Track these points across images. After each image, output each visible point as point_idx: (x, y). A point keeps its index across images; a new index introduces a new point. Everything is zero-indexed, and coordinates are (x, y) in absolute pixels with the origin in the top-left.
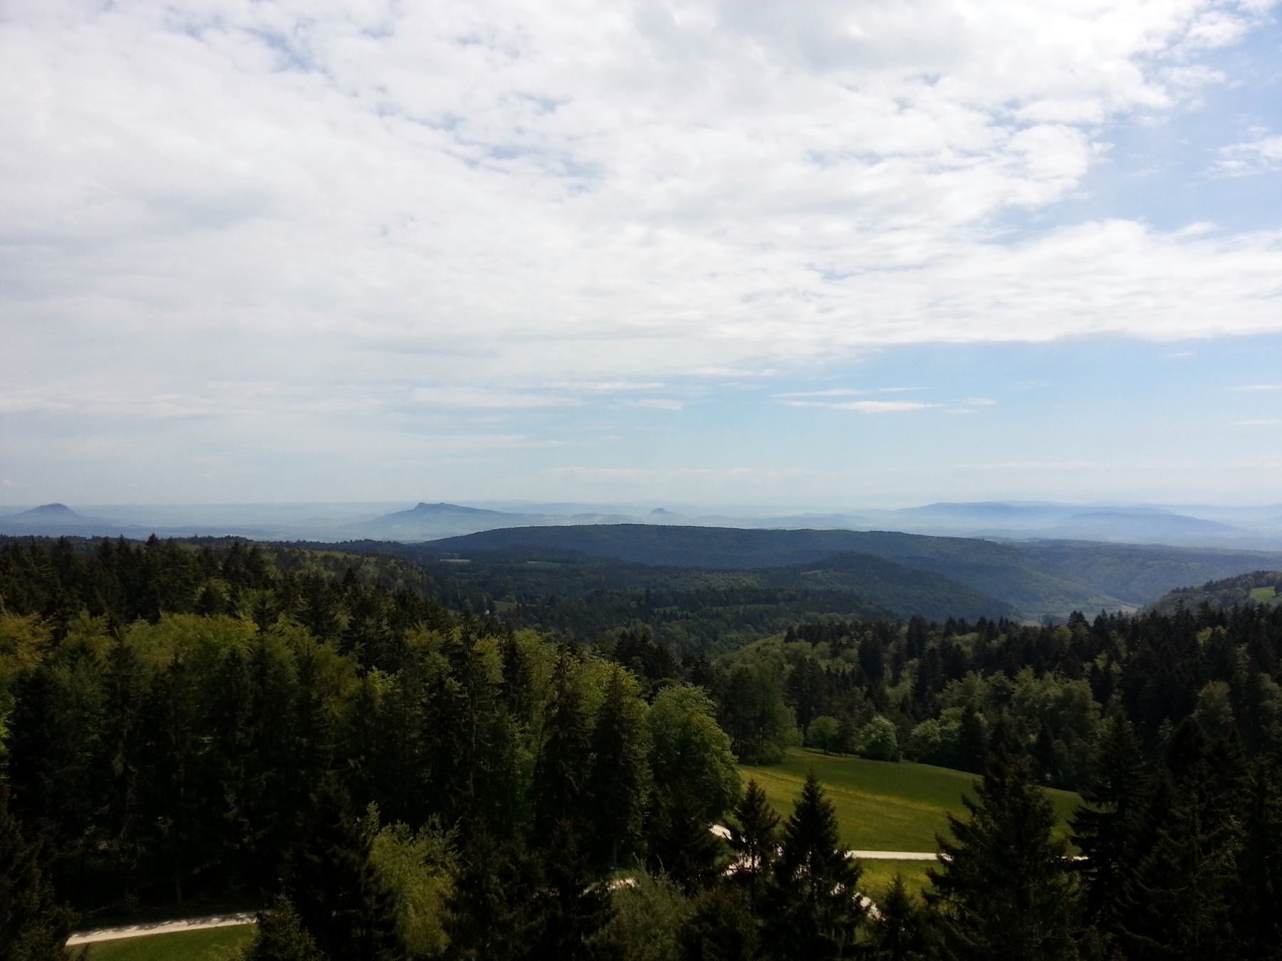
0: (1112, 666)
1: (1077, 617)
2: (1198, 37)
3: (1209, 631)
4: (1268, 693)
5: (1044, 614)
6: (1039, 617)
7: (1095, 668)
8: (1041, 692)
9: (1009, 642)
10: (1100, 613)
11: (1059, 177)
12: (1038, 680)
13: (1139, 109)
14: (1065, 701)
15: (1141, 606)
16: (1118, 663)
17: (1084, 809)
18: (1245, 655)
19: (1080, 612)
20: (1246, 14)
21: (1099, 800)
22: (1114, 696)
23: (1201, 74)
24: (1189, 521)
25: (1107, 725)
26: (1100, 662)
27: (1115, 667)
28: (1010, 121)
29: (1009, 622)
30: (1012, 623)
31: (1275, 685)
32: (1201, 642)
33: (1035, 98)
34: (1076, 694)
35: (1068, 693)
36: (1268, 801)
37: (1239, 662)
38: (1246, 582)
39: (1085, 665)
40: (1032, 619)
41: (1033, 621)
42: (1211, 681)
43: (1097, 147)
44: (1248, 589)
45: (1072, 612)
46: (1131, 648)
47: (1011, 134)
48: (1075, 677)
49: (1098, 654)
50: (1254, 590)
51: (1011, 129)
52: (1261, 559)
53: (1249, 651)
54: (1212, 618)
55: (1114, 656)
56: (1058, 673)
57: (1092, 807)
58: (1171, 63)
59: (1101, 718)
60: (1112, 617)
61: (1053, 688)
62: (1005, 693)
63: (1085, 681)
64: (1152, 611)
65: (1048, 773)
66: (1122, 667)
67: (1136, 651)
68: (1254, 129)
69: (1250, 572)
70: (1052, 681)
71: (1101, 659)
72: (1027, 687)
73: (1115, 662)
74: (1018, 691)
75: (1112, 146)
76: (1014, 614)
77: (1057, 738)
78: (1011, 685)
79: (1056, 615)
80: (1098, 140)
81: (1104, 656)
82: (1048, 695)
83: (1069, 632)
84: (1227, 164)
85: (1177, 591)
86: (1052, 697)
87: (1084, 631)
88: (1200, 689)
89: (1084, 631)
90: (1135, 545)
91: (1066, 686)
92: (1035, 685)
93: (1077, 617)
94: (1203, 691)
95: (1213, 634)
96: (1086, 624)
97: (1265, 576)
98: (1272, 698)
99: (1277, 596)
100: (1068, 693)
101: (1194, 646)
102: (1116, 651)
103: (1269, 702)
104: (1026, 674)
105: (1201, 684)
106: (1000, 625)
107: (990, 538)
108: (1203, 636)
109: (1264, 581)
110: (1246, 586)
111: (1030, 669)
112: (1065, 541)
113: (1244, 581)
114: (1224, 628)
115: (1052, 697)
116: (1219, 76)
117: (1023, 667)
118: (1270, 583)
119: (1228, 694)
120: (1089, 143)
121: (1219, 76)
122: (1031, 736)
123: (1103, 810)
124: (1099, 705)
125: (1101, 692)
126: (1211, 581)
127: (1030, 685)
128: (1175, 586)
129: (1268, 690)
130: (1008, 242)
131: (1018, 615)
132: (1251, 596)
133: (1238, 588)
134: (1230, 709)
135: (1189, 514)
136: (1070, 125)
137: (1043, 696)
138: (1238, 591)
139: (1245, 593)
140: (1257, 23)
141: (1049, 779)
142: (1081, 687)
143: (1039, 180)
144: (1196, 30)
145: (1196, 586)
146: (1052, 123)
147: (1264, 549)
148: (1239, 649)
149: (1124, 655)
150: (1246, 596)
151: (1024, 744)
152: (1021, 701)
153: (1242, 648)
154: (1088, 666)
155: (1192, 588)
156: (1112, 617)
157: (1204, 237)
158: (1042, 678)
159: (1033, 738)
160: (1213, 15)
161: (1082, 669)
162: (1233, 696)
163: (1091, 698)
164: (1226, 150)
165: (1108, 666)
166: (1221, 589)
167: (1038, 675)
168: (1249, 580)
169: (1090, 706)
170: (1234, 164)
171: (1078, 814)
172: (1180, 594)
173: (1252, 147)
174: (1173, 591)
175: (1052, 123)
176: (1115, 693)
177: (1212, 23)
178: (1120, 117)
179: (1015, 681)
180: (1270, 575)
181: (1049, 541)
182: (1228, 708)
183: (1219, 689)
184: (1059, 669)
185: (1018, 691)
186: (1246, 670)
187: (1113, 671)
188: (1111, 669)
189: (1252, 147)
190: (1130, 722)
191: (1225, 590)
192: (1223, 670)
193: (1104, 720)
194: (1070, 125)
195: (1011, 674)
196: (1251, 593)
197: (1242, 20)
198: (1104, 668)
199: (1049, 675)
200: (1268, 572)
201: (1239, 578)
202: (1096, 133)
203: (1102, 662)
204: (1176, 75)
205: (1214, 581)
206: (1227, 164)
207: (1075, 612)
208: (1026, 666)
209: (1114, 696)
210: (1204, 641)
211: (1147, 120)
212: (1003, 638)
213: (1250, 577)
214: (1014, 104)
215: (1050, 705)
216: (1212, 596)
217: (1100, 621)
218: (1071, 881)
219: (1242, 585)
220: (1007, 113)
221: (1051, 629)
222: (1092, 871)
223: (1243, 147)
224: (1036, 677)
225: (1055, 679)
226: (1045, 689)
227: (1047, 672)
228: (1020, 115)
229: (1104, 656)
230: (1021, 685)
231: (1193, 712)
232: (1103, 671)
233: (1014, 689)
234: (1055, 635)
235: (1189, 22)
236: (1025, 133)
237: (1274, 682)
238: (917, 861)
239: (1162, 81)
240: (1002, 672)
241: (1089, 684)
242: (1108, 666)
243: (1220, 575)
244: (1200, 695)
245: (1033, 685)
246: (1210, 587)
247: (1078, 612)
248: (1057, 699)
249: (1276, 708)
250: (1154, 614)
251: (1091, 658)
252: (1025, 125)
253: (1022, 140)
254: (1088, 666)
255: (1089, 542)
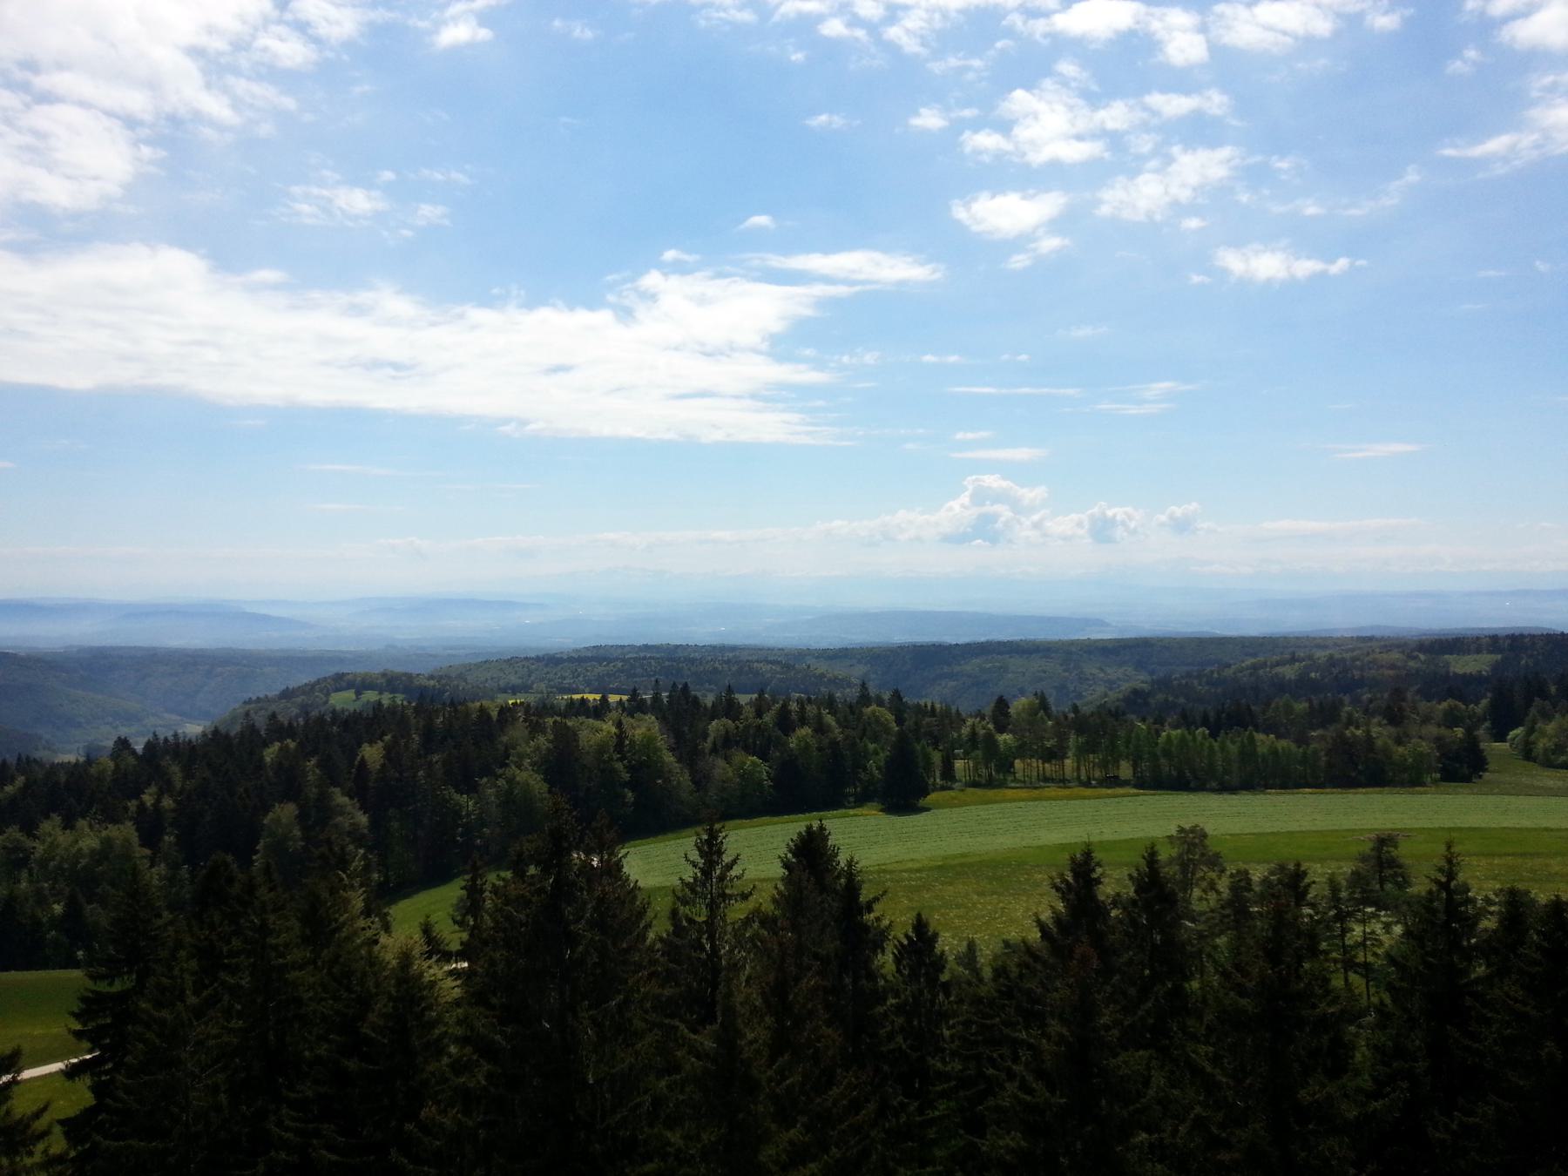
0: (163, 800)
1: (123, 744)
2: (265, 50)
3: (277, 745)
4: (339, 809)
5: (86, 744)
6: (78, 748)
7: (142, 806)
8: (71, 846)
9: (27, 786)
10: (150, 736)
11: (96, 178)
12: (68, 831)
13: (198, 117)
14: (104, 853)
15: (208, 723)
16: (171, 796)
17: (92, 992)
18: (316, 769)
19: (126, 738)
20: (318, 41)
21: (110, 978)
22: (166, 838)
23: (264, 92)
24: (507, 605)
25: (157, 874)
26: (148, 799)
27: (167, 803)
28: (25, 87)
29: (32, 759)
30: (35, 760)
31: (346, 799)
32: (268, 759)
33: (61, 66)
34: (118, 842)
35: (107, 843)
36: (272, 941)
37: (309, 778)
38: (325, 686)
39: (129, 804)
40: (70, 752)
41: (70, 755)
42: (277, 805)
43: (146, 151)
44: (328, 695)
45: (115, 739)
46: (188, 774)
47: (27, 106)
48: (116, 821)
49: (147, 788)
50: (333, 694)
51: (28, 99)
52: (338, 658)
53: (318, 765)
54: (279, 730)
55: (166, 788)
56: (94, 819)
57: (103, 987)
58: (236, 71)
59: (152, 866)
60: (166, 740)
61: (88, 839)
62: (21, 855)
63: (129, 824)
64: (213, 729)
65: (79, 950)
66: (175, 801)
67: (193, 779)
68: (326, 173)
69: (330, 674)
70: (87, 830)
71: (150, 795)
72: (52, 843)
73: (166, 796)
74: (40, 848)
75: (164, 154)
76: (44, 749)
77: (89, 903)
78: (29, 843)
79: (101, 744)
80: (148, 142)
81: (153, 789)
82: (81, 849)
83: (111, 765)
84: (298, 206)
85: (250, 701)
86: (86, 850)
87: (131, 760)
88: (265, 815)
89: (131, 760)
90: (201, 650)
91: (104, 833)
92: (64, 838)
93: (123, 744)
94: (269, 817)
95: (281, 749)
96: (134, 752)
97: (345, 678)
98: (342, 814)
99: (358, 699)
100: (107, 843)
101: (260, 765)
102: (169, 782)
103: (340, 818)
104: (50, 827)
105: (267, 809)
106: (18, 764)
107: (9, 648)
108: (270, 754)
109: (344, 684)
110: (325, 691)
111: (57, 818)
112: (112, 648)
113: (323, 685)
114: (294, 741)
115: (86, 850)
116: (289, 103)
117: (47, 817)
118: (350, 686)
119: (297, 817)
120: (136, 143)
121: (289, 103)
122: (56, 906)
123: (117, 987)
124: (147, 852)
125: (150, 830)
126: (287, 688)
127: (55, 839)
128: (246, 696)
129: (338, 805)
130: (25, 250)
131: (49, 749)
132: (330, 702)
133: (317, 694)
134: (299, 833)
135: (263, 611)
136: (109, 114)
137: (74, 850)
138: (317, 697)
139: (324, 699)
140: (329, 54)
141: (82, 957)
142: (125, 832)
143: (69, 177)
144: (264, 41)
145: (271, 694)
146: (84, 104)
147: (344, 648)
148: (308, 764)
149: (178, 785)
150: (326, 702)
151: (45, 920)
152: (43, 863)
153: (312, 762)
154: (132, 805)
155: (266, 696)
156: (166, 740)
157: (275, 287)
158: (72, 828)
159: (58, 908)
160: (281, 30)
161: (126, 809)
162: (302, 817)
163: (137, 844)
164: (296, 190)
165: (158, 801)
166: (298, 696)
167: (68, 824)
168: (329, 683)
169: (137, 855)
170: (305, 208)
171: (84, 999)
172: (253, 706)
173: (325, 193)
174: (245, 703)
175: (84, 104)
176: (167, 834)
177: (281, 39)
178: (174, 120)
179: (35, 837)
180: (350, 677)
181: (91, 650)
182: (297, 833)
183: (285, 812)
184: (95, 813)
185: (40, 848)
186: (316, 787)
187: (163, 807)
188: (161, 804)
189: (325, 193)
190: (186, 866)
191: (303, 697)
192: (290, 786)
193: (153, 870)
194: (109, 114)
195: (29, 828)
196: (331, 699)
197: (313, 46)
198: (153, 805)
199: (82, 823)
200: (349, 674)
201: (318, 682)
202: (144, 132)
203: (151, 798)
204: (241, 86)
205: (291, 687)
206: (298, 206)
207: (119, 738)
208: (52, 815)
209: (166, 838)
210: (272, 759)
211: (208, 133)
212: (20, 780)
213: (329, 680)
214: (31, 66)
215: (83, 862)
216: (289, 705)
217: (149, 746)
218: (782, 923)
219: (321, 691)
220: (19, 75)
221: (89, 762)
222: (106, 1067)
223: (315, 191)
224: (65, 828)
225: (91, 827)
226: (77, 842)
227: (80, 819)
228: (41, 82)
229: (153, 789)
230: (43, 842)
231: (258, 843)
232: (151, 808)
233: (34, 848)
234: (93, 771)
235: (256, 29)
236: (45, 108)
237: (346, 796)
238: (51, 1075)
239: (226, 90)
240: (17, 827)
241: (134, 827)
242: (158, 801)
243: (303, 679)
244: (265, 822)
245: (61, 839)
246: (287, 694)
247: (123, 737)
248: (93, 851)
249: (347, 825)
250: (216, 732)
251: (137, 793)
252: (47, 98)
253: (42, 118)
254: (132, 805)
255: (141, 649)
